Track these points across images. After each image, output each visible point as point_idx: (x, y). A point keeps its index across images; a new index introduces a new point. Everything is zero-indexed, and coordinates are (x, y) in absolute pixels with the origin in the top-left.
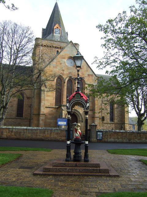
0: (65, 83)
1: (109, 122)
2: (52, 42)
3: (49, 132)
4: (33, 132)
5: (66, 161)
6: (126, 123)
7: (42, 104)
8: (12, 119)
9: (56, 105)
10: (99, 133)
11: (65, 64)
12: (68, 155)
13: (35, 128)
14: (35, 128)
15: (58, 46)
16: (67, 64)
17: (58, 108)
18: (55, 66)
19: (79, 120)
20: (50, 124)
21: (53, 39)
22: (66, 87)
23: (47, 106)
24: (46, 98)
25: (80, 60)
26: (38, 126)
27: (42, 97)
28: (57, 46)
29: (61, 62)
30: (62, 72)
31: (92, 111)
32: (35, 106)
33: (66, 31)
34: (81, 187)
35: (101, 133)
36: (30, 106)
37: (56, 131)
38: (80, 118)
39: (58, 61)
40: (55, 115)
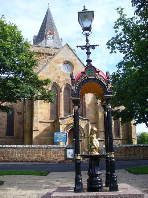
0: (61, 91)
2: (45, 49)
3: (44, 152)
4: (24, 152)
6: (133, 137)
7: (35, 118)
8: (6, 139)
9: (51, 119)
11: (61, 70)
13: (27, 146)
14: (27, 146)
15: (52, 53)
16: (62, 70)
17: (53, 122)
18: (49, 72)
20: (46, 142)
21: (47, 46)
22: (63, 101)
23: (41, 121)
24: (40, 110)
25: (89, 20)
26: (31, 144)
27: (35, 110)
28: (51, 53)
29: (56, 67)
30: (57, 78)
31: (95, 125)
32: (27, 121)
33: (60, 38)
34: (5, 65)
36: (22, 123)
38: (81, 134)
39: (52, 67)
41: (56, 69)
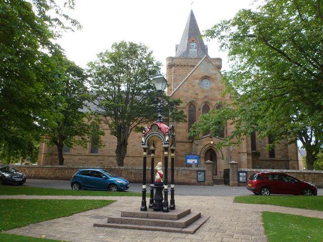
1: (269, 159)
5: (142, 210)
10: (241, 174)
12: (144, 203)
18: (186, 89)
19: (218, 156)
29: (194, 84)
35: (245, 174)
37: (184, 172)
40: (188, 151)
41: (193, 86)
